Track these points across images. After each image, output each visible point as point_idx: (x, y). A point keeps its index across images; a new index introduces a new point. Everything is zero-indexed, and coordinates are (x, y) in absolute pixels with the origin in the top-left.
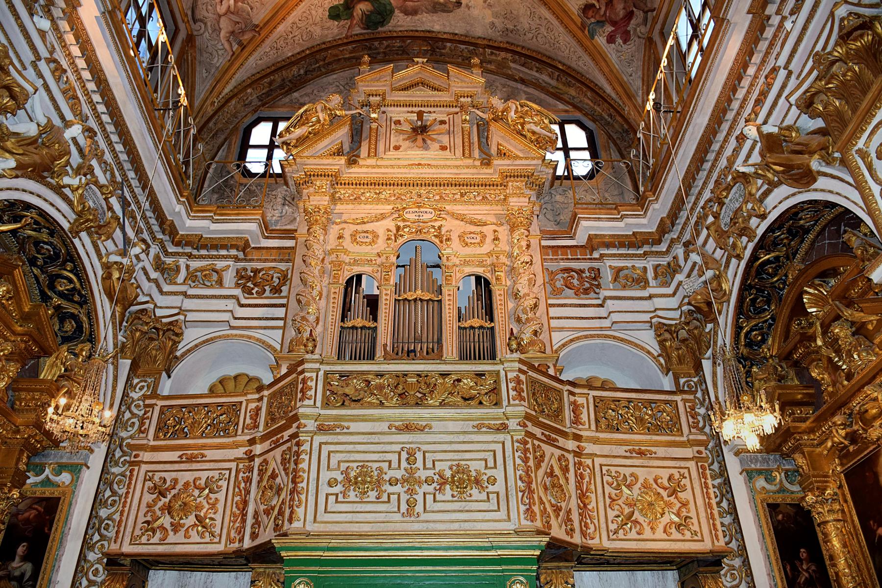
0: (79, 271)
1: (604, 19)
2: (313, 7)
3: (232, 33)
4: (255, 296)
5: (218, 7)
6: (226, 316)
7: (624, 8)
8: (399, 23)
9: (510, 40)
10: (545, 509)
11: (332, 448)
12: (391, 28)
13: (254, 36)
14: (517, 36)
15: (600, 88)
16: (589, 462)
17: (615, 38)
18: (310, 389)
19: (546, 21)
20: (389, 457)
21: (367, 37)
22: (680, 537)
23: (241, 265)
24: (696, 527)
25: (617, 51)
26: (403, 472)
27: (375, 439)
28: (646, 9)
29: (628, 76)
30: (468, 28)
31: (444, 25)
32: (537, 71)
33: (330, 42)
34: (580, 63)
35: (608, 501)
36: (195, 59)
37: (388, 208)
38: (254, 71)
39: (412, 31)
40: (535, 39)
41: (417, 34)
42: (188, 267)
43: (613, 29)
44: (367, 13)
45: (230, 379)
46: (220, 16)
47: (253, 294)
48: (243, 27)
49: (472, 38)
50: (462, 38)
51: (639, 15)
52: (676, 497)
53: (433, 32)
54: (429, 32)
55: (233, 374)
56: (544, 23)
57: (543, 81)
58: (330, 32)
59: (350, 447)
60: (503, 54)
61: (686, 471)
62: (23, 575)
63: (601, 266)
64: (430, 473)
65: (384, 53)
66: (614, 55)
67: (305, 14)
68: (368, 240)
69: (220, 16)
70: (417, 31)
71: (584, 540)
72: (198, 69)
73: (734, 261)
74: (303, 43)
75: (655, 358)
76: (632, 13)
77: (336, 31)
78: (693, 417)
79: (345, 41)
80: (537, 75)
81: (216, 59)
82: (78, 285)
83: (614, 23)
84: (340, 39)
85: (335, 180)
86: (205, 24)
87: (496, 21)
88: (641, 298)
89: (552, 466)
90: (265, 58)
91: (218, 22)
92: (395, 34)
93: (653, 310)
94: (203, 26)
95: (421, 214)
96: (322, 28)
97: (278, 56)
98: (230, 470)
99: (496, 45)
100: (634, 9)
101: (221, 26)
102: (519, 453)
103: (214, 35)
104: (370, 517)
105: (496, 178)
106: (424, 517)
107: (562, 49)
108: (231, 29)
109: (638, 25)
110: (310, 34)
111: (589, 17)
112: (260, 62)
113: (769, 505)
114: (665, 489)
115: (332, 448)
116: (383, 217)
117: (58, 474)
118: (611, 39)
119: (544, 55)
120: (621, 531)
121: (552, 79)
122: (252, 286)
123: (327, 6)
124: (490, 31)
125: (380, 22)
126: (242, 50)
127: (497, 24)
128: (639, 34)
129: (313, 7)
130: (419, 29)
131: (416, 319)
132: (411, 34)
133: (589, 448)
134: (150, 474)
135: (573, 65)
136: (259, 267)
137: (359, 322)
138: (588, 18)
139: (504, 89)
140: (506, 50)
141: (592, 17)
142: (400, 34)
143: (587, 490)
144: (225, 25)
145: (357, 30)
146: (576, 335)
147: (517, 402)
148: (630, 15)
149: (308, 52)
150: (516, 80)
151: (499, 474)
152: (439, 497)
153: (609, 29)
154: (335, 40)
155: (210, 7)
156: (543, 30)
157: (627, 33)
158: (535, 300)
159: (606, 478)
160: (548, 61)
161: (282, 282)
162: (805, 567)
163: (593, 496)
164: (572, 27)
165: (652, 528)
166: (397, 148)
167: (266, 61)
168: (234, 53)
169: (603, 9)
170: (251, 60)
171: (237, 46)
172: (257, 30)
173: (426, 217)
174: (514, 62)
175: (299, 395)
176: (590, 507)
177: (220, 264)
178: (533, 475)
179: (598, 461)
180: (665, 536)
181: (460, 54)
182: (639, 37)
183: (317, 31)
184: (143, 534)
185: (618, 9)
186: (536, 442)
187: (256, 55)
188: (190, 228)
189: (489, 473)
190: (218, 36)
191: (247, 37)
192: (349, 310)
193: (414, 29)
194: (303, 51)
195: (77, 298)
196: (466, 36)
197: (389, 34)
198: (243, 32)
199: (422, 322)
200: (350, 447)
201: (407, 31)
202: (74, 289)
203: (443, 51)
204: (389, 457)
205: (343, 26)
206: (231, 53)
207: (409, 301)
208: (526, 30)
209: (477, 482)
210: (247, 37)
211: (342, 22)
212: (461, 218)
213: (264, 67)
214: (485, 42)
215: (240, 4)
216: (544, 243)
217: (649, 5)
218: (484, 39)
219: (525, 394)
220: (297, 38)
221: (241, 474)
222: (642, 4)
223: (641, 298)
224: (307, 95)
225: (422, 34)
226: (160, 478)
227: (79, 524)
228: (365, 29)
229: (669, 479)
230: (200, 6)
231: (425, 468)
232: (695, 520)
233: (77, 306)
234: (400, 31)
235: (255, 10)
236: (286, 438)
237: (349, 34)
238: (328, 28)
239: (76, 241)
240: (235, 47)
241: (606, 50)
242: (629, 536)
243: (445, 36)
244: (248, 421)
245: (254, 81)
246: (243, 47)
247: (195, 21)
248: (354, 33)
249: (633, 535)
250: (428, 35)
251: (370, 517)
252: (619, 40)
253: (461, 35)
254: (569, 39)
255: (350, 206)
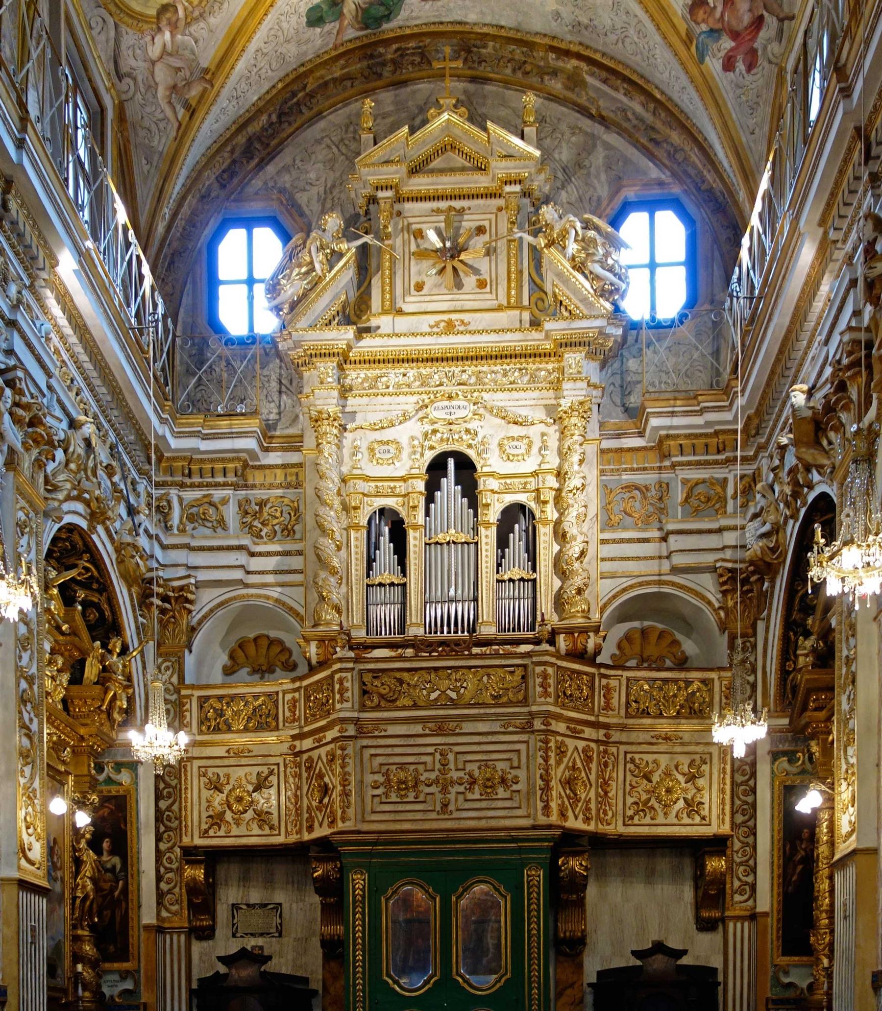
0: (96, 560)
1: (719, 26)
2: (283, 18)
3: (174, 87)
4: (265, 539)
5: (150, 49)
6: (238, 575)
7: (750, 10)
8: (414, 14)
9: (587, 42)
10: (563, 802)
11: (373, 751)
12: (401, 23)
13: (205, 90)
14: (594, 36)
15: (711, 147)
16: (614, 750)
17: (735, 61)
18: (347, 690)
19: (636, 19)
20: (424, 759)
21: (366, 41)
22: (689, 821)
23: (243, 493)
24: (705, 813)
25: (738, 86)
26: (437, 773)
27: (411, 741)
28: (781, 16)
29: (748, 133)
30: (520, 18)
31: (482, 12)
32: (625, 95)
33: (310, 60)
34: (685, 97)
35: (628, 788)
36: (128, 141)
37: (409, 403)
38: (211, 141)
39: (434, 23)
40: (620, 44)
41: (442, 28)
42: (181, 499)
43: (733, 44)
44: (364, 6)
45: (249, 641)
46: (153, 63)
47: (262, 537)
48: (188, 74)
49: (527, 33)
50: (511, 34)
51: (771, 22)
52: (694, 784)
53: (466, 23)
54: (460, 23)
55: (252, 636)
56: (634, 22)
57: (634, 113)
58: (310, 45)
59: (389, 751)
60: (574, 62)
61: (708, 756)
62: (114, 867)
63: (671, 478)
64: (461, 774)
65: (393, 61)
66: (731, 95)
67: (272, 32)
68: (389, 456)
69: (153, 63)
70: (442, 23)
71: (600, 826)
72: (135, 159)
73: (791, 522)
74: (274, 74)
75: (715, 610)
76: (761, 18)
77: (319, 42)
78: (727, 698)
79: (334, 53)
80: (625, 99)
81: (157, 137)
82: (96, 573)
83: (735, 35)
84: (326, 52)
85: (344, 360)
86: (135, 79)
87: (561, 9)
88: (710, 531)
89: (574, 760)
90: (223, 117)
91: (153, 74)
92: (408, 31)
93: (720, 546)
94: (132, 83)
95: (452, 411)
96: (299, 43)
97: (239, 108)
98: (278, 764)
99: (563, 46)
100: (766, 14)
101: (157, 79)
102: (541, 753)
103: (149, 96)
104: (410, 816)
105: (548, 346)
106: (456, 815)
107: (660, 69)
108: (171, 82)
109: (769, 40)
110: (282, 57)
111: (699, 20)
112: (216, 126)
113: (785, 787)
114: (684, 775)
115: (373, 751)
116: (405, 417)
117: (119, 771)
118: (728, 65)
119: (635, 71)
120: (636, 817)
121: (647, 110)
122: (260, 526)
123: (303, 9)
124: (554, 24)
125: (385, 16)
126: (190, 118)
127: (564, 15)
128: (770, 56)
129: (283, 18)
130: (444, 19)
131: (450, 565)
132: (433, 28)
133: (616, 736)
134: (203, 770)
135: (675, 97)
136: (264, 497)
137: (387, 578)
138: (698, 24)
139: (574, 139)
140: (579, 56)
141: (703, 21)
142: (416, 30)
143: (609, 779)
144: (161, 75)
145: (351, 33)
146: (630, 583)
147: (543, 699)
148: (758, 22)
149: (280, 86)
150: (591, 117)
151: (522, 774)
152: (470, 796)
153: (727, 44)
154: (318, 56)
155: (138, 51)
156: (632, 32)
157: (753, 52)
158: (582, 546)
159: (629, 766)
160: (640, 82)
161: (293, 518)
162: (803, 846)
163: (614, 784)
164: (675, 40)
165: (665, 814)
166: (419, 287)
167: (226, 120)
168: (180, 125)
169: (720, 9)
170: (205, 127)
171: (183, 110)
172: (208, 77)
173: (460, 414)
174: (592, 74)
175: (337, 696)
176: (610, 795)
177: (218, 494)
178: (553, 773)
179: (623, 748)
180: (675, 821)
181: (510, 56)
182: (770, 62)
183: (292, 51)
184: (210, 828)
185: (741, 11)
186: (559, 738)
187: (210, 118)
188: (177, 450)
189: (514, 772)
190: (155, 96)
191: (194, 92)
192: (374, 560)
193: (437, 20)
194: (274, 87)
195: (95, 586)
196: (518, 31)
197: (400, 33)
198: (189, 84)
199: (456, 563)
200: (389, 751)
201: (426, 24)
202: (92, 577)
203: (484, 51)
204: (424, 759)
205: (329, 33)
206: (176, 125)
207: (441, 544)
208: (607, 27)
209: (503, 781)
210: (194, 92)
211: (328, 27)
212: (502, 415)
213: (221, 131)
214: (546, 41)
215: (179, 37)
216: (606, 444)
217: (786, 9)
218: (545, 35)
219: (551, 690)
220: (264, 70)
221: (289, 770)
222: (775, 6)
223: (710, 531)
224: (286, 169)
225: (450, 28)
226: (213, 774)
227: (147, 816)
228: (362, 29)
229: (690, 766)
230: (125, 53)
231: (457, 770)
232: (707, 806)
233: (97, 595)
234: (416, 26)
235: (201, 43)
236: (329, 739)
237: (339, 42)
238: (308, 41)
239: (94, 537)
240: (181, 112)
241: (720, 85)
242: (644, 822)
243: (485, 30)
244: (288, 714)
245: (210, 158)
246: (192, 112)
247: (120, 77)
248: (346, 38)
249: (648, 820)
250: (458, 28)
251: (410, 816)
252: (741, 66)
253: (510, 29)
254: (668, 55)
255: (365, 400)
